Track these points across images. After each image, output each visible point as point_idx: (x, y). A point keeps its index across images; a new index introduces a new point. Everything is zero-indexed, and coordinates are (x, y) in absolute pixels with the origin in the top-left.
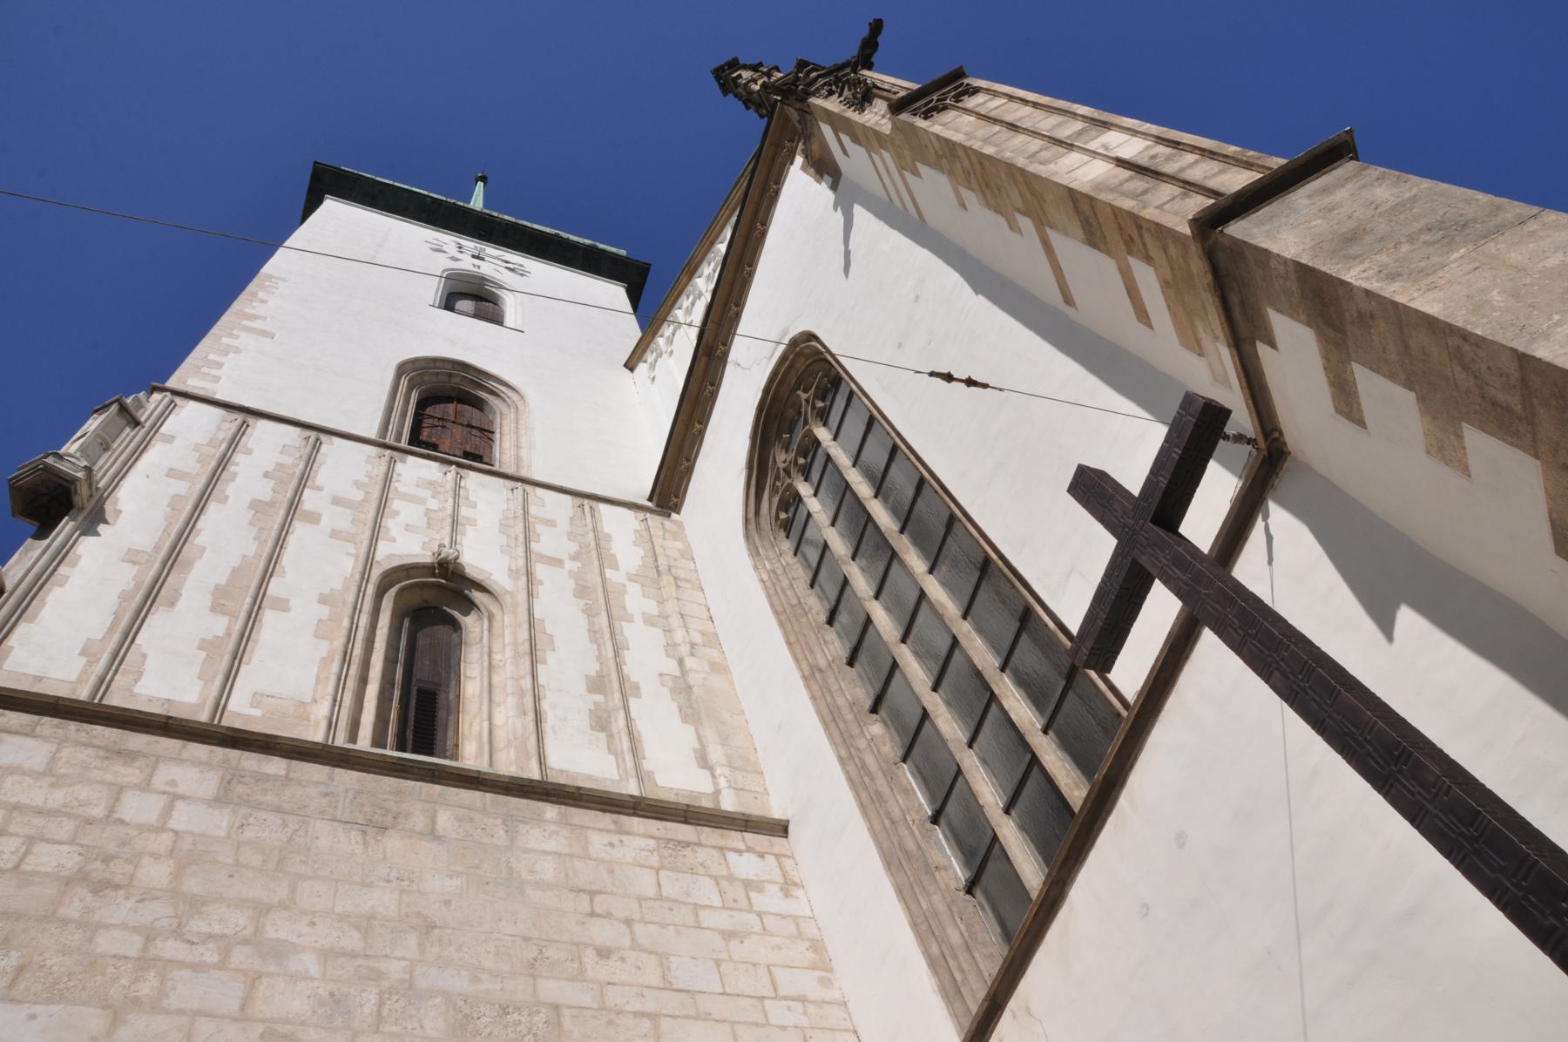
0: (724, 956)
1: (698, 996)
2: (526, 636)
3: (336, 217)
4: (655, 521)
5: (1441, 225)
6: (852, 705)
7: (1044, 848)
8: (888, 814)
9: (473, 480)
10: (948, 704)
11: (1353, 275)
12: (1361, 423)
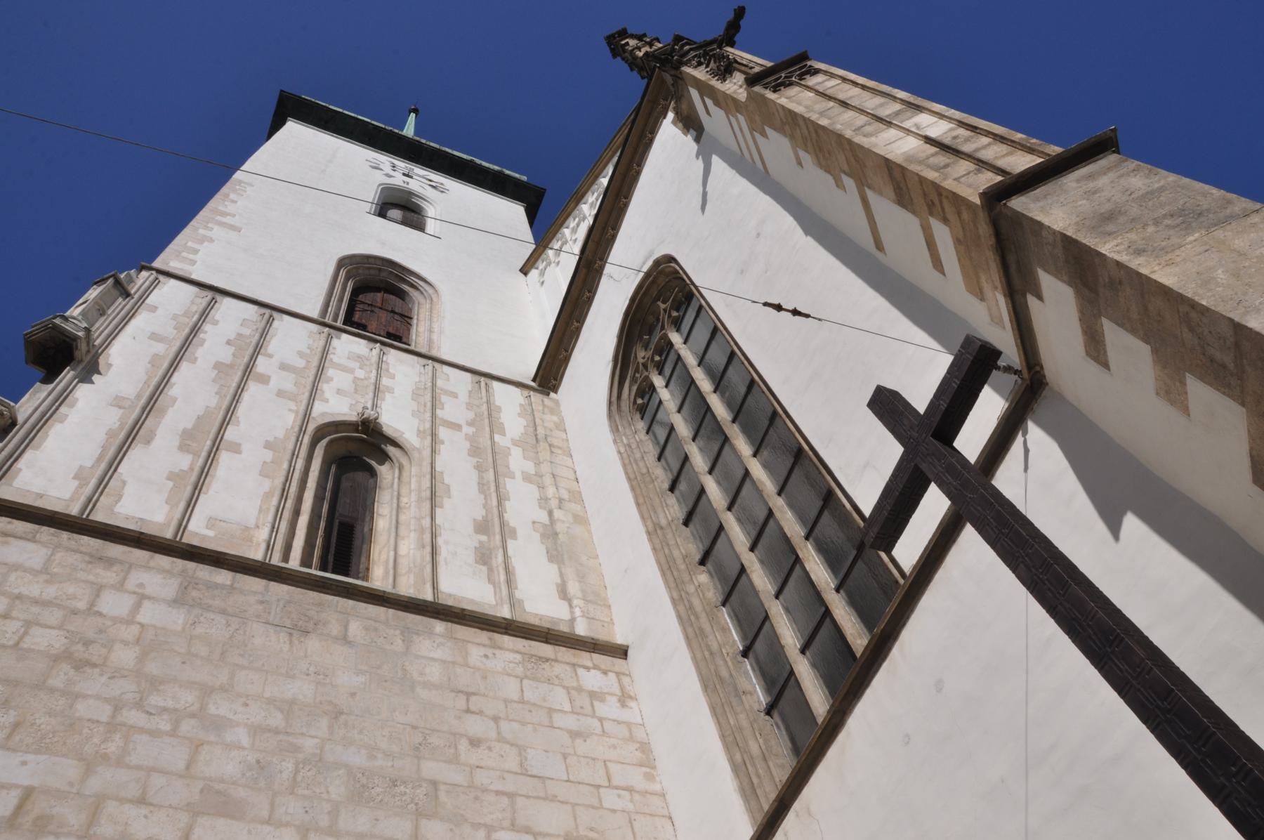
0: (571, 751)
1: (548, 782)
2: (428, 485)
3: (296, 135)
4: (536, 398)
5: (1181, 212)
6: (685, 557)
7: (830, 681)
8: (708, 646)
9: (393, 356)
10: (762, 562)
11: (1108, 248)
12: (1106, 365)
